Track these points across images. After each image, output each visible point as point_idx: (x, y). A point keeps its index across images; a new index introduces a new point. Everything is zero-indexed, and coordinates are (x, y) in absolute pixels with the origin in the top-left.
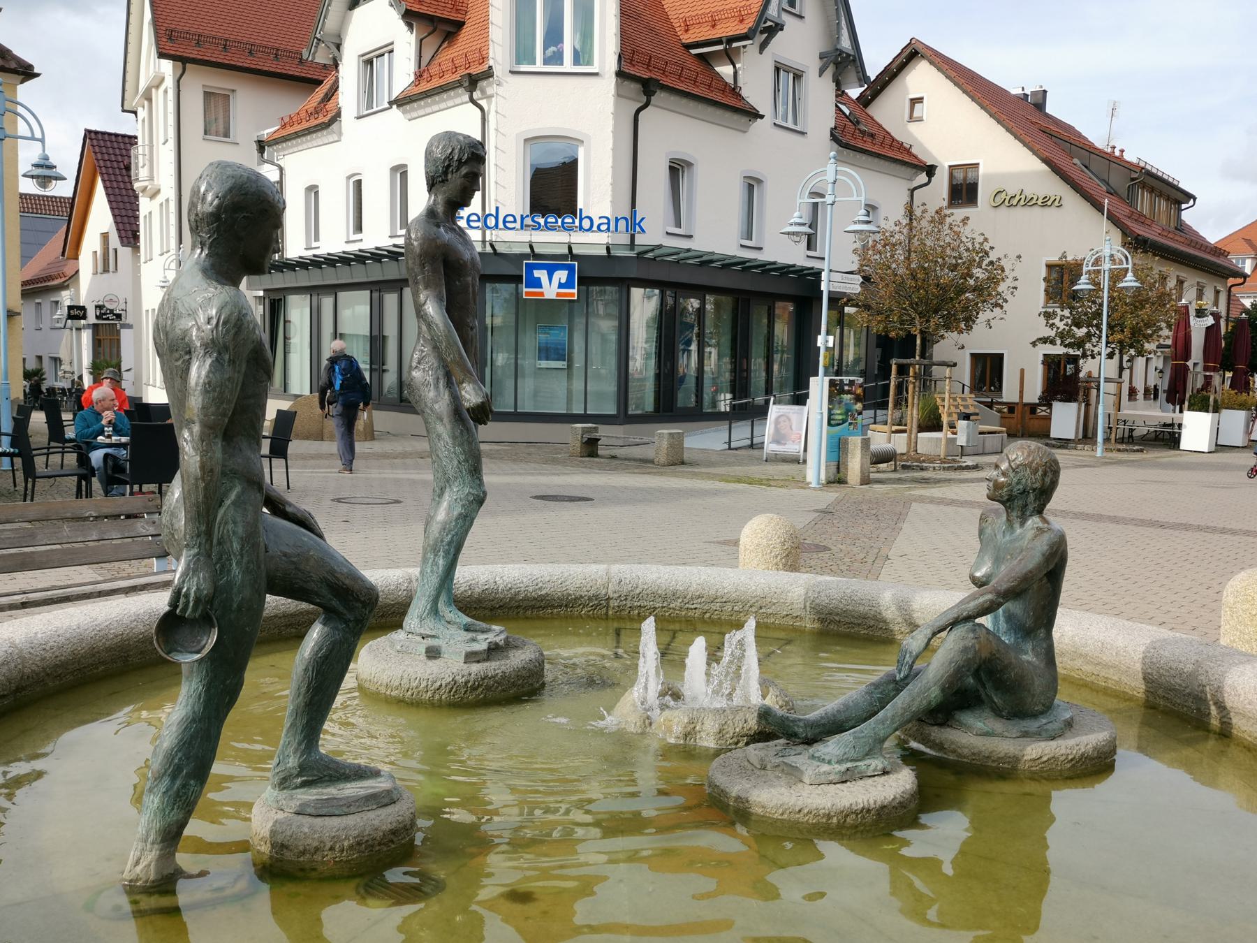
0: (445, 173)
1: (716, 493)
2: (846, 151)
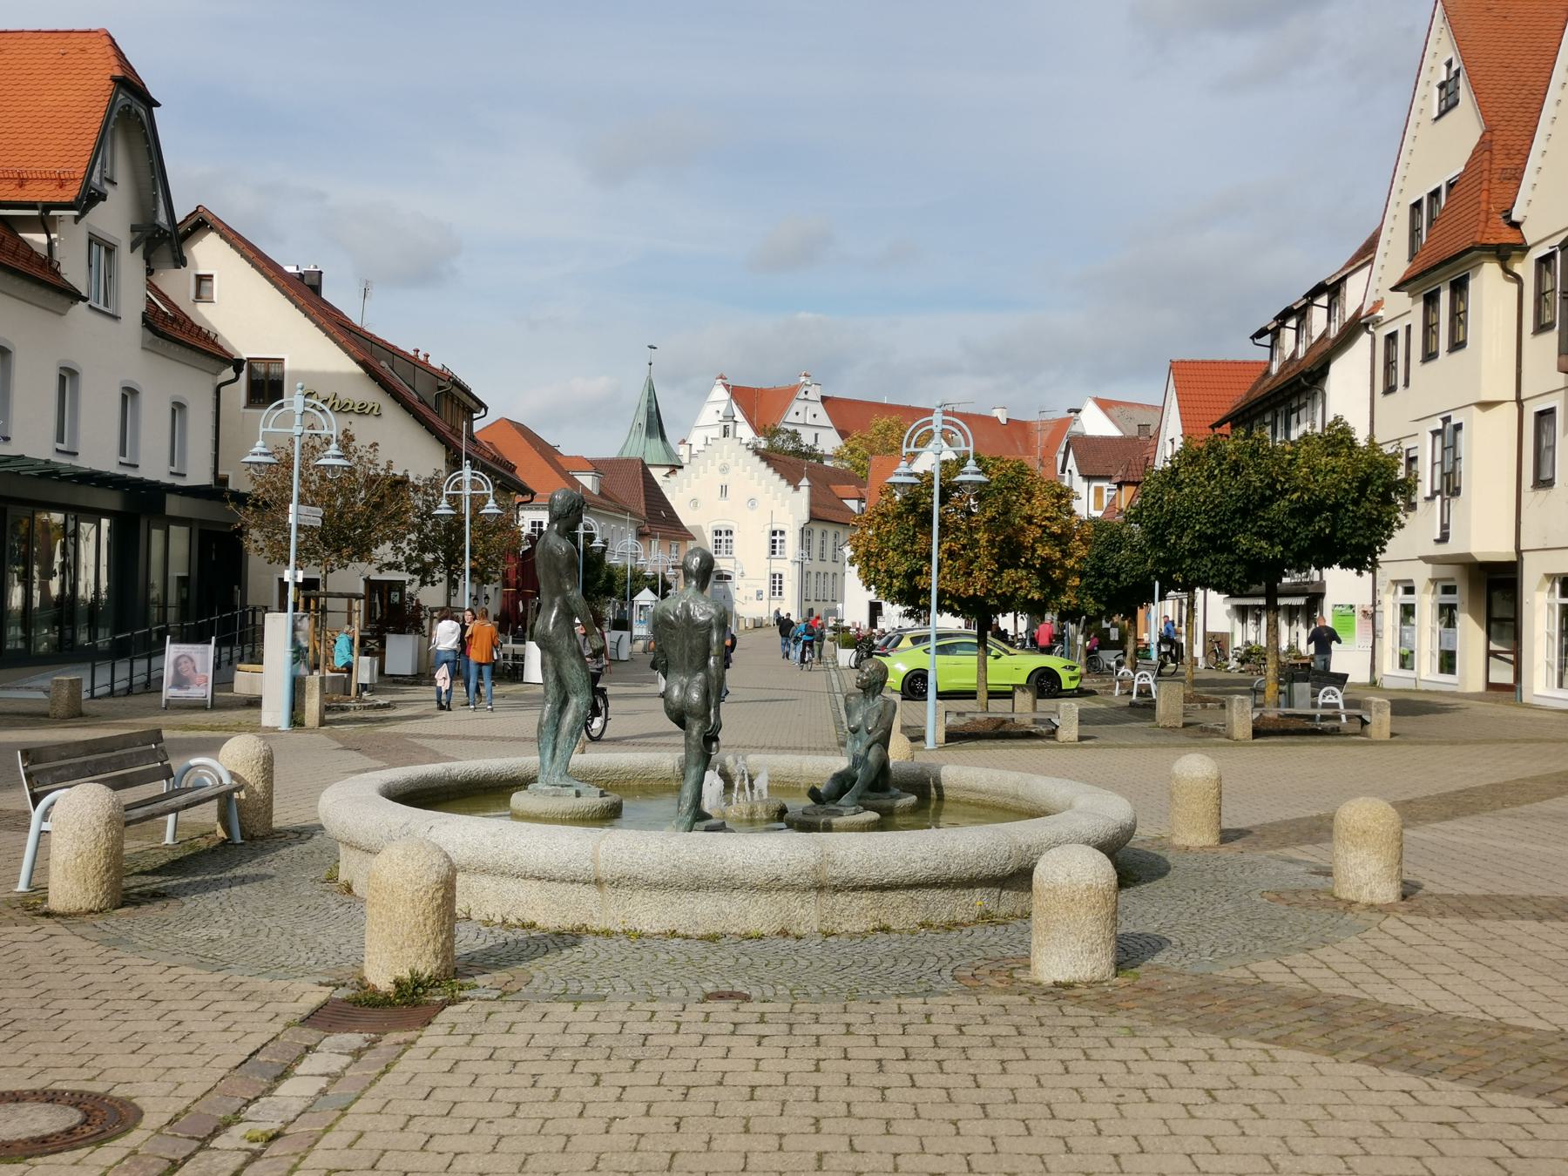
2: (161, 341)
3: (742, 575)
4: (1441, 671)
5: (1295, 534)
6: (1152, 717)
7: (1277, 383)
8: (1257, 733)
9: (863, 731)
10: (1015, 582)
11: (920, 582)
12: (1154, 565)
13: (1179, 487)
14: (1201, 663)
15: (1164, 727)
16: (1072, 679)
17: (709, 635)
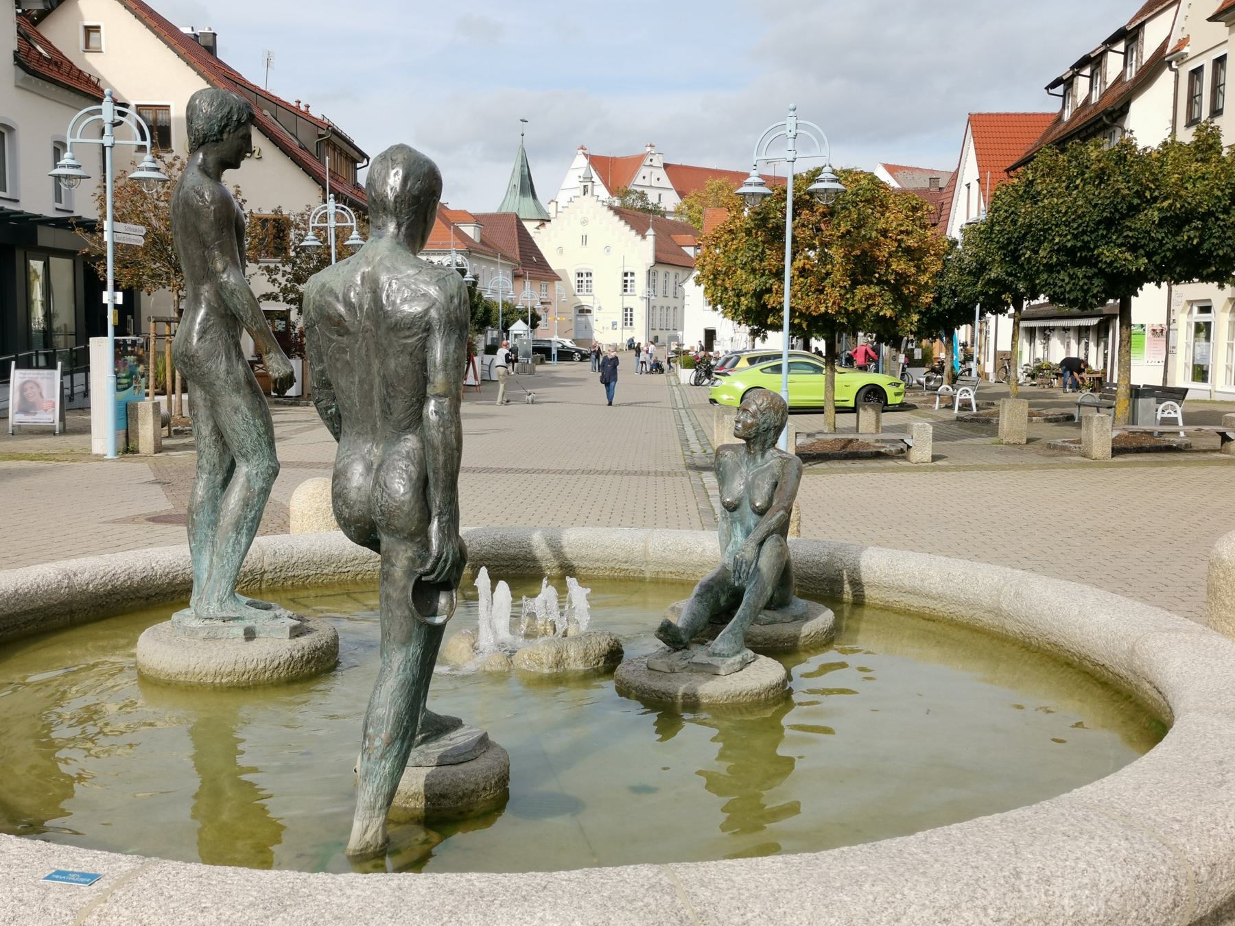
0: (221, 132)
1: (38, 471)
2: (34, 79)
3: (600, 308)
4: (1193, 380)
5: (1161, 245)
6: (994, 432)
7: (1069, 129)
8: (1116, 451)
9: (746, 508)
10: (867, 299)
11: (771, 300)
12: (984, 286)
13: (1035, 199)
14: (992, 378)
15: (1008, 444)
16: (897, 394)
17: (424, 347)
